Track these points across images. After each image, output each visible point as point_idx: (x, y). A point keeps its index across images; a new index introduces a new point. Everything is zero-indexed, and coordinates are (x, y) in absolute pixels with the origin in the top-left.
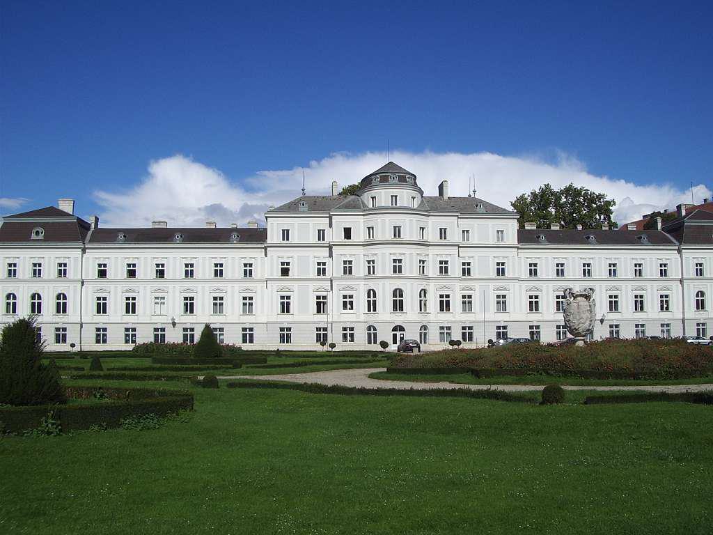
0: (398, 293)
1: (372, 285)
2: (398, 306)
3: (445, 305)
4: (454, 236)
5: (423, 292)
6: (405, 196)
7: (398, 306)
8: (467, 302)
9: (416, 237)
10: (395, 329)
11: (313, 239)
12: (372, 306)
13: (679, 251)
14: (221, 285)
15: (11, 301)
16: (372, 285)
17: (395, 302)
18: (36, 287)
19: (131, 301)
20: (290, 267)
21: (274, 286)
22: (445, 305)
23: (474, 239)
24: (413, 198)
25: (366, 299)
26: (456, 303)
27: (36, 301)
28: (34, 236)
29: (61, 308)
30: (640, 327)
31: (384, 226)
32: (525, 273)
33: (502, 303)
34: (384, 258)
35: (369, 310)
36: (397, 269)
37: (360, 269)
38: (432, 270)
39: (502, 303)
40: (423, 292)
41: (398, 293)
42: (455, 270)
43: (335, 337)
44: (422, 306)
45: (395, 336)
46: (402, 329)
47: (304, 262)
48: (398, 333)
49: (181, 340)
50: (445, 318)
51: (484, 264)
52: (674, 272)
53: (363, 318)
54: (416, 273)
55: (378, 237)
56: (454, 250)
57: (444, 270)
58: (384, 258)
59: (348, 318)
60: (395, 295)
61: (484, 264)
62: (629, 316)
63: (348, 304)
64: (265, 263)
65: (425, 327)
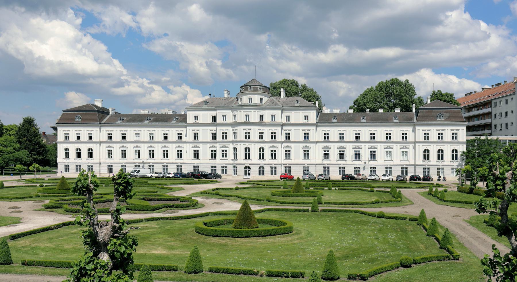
0: (247, 149)
1: (247, 145)
2: (247, 156)
4: (267, 119)
7: (247, 156)
15: (426, 153)
17: (246, 154)
18: (78, 145)
19: (196, 152)
20: (360, 135)
21: (104, 145)
23: (200, 121)
25: (258, 152)
27: (247, 152)
28: (77, 120)
29: (91, 155)
30: (165, 168)
32: (353, 139)
33: (306, 154)
36: (247, 136)
38: (267, 137)
39: (306, 154)
45: (246, 171)
46: (249, 168)
47: (205, 134)
48: (247, 170)
49: (192, 171)
50: (274, 162)
51: (297, 134)
52: (410, 138)
53: (231, 162)
55: (252, 120)
56: (230, 128)
59: (224, 162)
60: (246, 150)
61: (297, 134)
64: (188, 133)
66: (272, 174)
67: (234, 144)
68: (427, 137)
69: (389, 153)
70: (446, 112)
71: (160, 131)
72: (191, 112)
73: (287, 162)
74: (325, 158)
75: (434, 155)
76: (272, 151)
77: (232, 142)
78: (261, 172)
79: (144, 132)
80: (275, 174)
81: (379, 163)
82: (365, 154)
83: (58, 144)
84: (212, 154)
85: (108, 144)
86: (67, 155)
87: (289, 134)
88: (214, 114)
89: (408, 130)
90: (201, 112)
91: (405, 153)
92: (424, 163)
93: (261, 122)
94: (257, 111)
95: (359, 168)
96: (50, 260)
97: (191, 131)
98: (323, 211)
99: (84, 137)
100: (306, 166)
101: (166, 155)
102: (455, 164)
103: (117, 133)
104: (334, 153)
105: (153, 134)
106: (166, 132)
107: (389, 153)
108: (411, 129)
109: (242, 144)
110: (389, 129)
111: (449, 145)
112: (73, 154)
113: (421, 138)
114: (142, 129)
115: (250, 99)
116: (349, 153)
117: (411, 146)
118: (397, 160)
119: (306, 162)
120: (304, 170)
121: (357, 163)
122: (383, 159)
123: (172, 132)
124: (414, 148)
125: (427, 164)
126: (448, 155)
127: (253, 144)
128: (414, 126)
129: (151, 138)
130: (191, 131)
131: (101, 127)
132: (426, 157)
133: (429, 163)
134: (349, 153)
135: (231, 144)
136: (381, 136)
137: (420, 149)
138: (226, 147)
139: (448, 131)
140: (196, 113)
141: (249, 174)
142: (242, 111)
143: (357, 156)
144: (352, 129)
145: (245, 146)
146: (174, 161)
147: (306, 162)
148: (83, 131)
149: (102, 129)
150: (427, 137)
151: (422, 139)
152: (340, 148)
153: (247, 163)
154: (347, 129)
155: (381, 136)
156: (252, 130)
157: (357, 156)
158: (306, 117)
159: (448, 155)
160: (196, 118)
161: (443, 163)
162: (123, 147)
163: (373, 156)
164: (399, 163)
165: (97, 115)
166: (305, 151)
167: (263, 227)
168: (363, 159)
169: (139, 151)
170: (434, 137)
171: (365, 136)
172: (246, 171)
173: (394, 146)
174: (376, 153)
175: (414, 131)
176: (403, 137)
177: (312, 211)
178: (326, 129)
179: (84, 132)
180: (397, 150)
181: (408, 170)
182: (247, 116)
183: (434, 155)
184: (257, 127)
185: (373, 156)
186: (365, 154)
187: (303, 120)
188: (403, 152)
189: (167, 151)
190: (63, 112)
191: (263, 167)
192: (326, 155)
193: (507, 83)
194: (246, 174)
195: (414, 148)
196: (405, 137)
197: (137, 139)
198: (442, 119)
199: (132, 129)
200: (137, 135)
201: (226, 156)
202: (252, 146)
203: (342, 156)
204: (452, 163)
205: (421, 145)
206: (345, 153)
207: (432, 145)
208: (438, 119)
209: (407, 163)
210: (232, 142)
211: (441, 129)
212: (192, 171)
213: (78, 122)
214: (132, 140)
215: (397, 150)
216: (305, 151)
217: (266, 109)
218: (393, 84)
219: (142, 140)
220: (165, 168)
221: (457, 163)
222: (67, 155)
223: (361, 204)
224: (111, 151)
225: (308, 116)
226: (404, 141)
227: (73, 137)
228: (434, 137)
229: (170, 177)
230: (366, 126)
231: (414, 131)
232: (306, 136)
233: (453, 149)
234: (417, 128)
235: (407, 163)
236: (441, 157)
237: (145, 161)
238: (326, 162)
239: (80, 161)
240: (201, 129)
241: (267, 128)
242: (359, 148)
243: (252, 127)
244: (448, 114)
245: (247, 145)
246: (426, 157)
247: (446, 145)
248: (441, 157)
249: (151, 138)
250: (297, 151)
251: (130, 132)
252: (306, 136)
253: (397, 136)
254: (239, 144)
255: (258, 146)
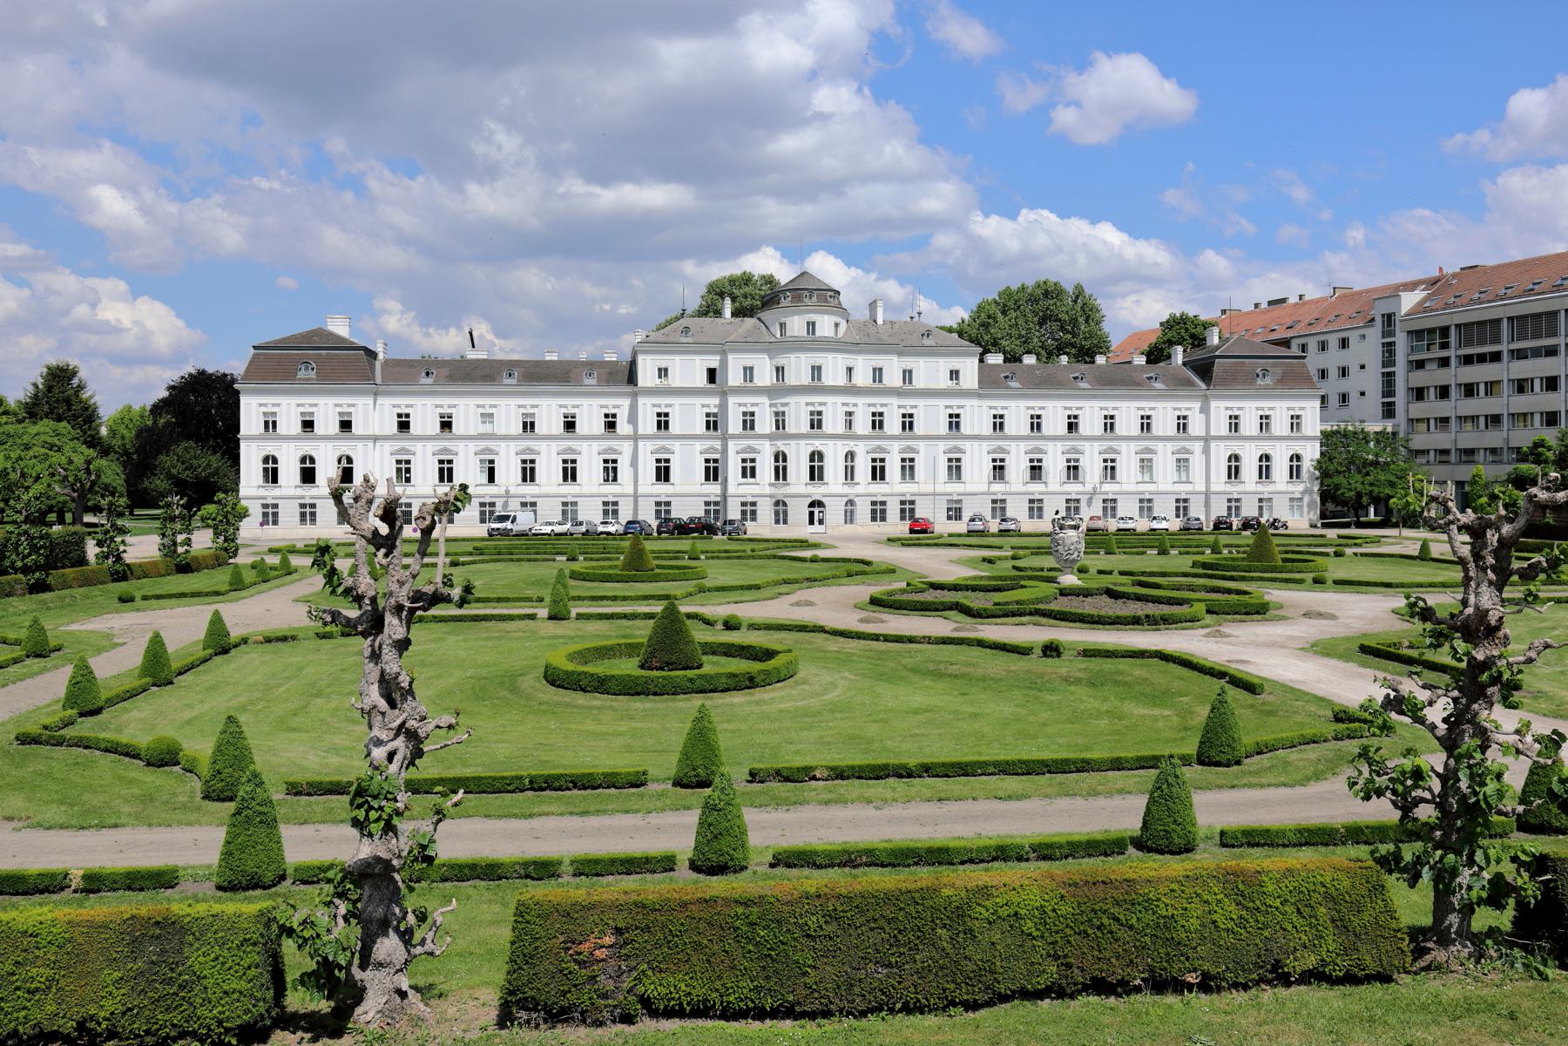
0: (817, 456)
1: (818, 445)
2: (816, 474)
3: (878, 473)
4: (893, 379)
5: (850, 456)
6: (826, 325)
7: (816, 474)
8: (908, 468)
9: (841, 380)
10: (812, 505)
11: (701, 380)
12: (781, 473)
13: (1206, 400)
14: (614, 444)
16: (781, 445)
18: (307, 447)
20: (411, 419)
22: (878, 473)
23: (675, 380)
24: (837, 325)
25: (773, 464)
26: (893, 469)
28: (301, 374)
30: (569, 509)
31: (798, 368)
33: (955, 468)
34: (798, 412)
35: (777, 478)
36: (816, 423)
37: (765, 424)
38: (862, 425)
39: (955, 468)
40: (850, 456)
41: (817, 456)
42: (893, 425)
43: (1127, 508)
44: (850, 473)
47: (689, 416)
48: (816, 511)
49: (701, 514)
50: (879, 489)
51: (931, 416)
52: (1196, 426)
53: (768, 490)
54: (840, 429)
55: (791, 379)
56: (764, 400)
57: (878, 422)
58: (798, 412)
59: (749, 489)
60: (777, 460)
61: (931, 416)
62: (553, 490)
63: (749, 471)
65: (851, 502)
66: (874, 519)
67: (779, 443)
68: (1235, 423)
69: (1146, 465)
70: (1274, 365)
71: (554, 408)
72: (649, 358)
73: (908, 489)
74: (1033, 478)
75: (1249, 468)
76: (874, 460)
77: (770, 437)
78: (781, 515)
79: (508, 410)
80: (1040, 517)
81: (1125, 488)
82: (1092, 466)
83: (243, 445)
84: (565, 470)
85: (606, 444)
86: (272, 476)
87: (820, 413)
88: (714, 361)
89: (1192, 408)
90: (677, 358)
91: (1182, 464)
92: (1229, 488)
93: (816, 386)
94: (840, 356)
95: (1078, 501)
96: (954, 760)
97: (649, 406)
98: (580, 617)
99: (327, 423)
100: (955, 497)
101: (570, 474)
102: (1298, 488)
103: (425, 413)
104: (1017, 467)
105: (274, 414)
106: (572, 411)
107: (1146, 465)
108: (1197, 405)
109: (803, 442)
110: (1146, 406)
111: (1284, 444)
112: (289, 472)
113: (1220, 426)
114: (502, 402)
115: (811, 326)
116: (1055, 465)
117: (1197, 447)
118: (1165, 480)
119: (955, 488)
120: (949, 509)
121: (1073, 488)
122: (1133, 480)
123: (590, 413)
124: (1206, 451)
125: (1234, 489)
126: (1280, 468)
127: (830, 443)
128: (1206, 400)
129: (529, 426)
130: (647, 410)
131: (376, 394)
132: (1234, 472)
133: (1240, 488)
134: (1055, 465)
135: (767, 443)
136: (1127, 421)
137: (1221, 453)
138: (754, 450)
139: (1281, 410)
140: (663, 360)
141: (821, 522)
142: (803, 356)
143: (1073, 470)
144: (1060, 404)
145: (811, 449)
146: (595, 489)
147: (955, 488)
148: (284, 407)
149: (380, 400)
150: (1235, 423)
151: (1224, 431)
152: (1031, 452)
153: (817, 491)
154: (1123, 405)
155: (1127, 421)
156: (830, 405)
157: (1073, 470)
158: (954, 374)
159: (1280, 468)
160: (663, 372)
161: (1271, 488)
162: (403, 451)
163: (1110, 471)
164: (1170, 488)
165: (345, 364)
166: (950, 460)
167: (712, 666)
168: (1088, 478)
169: (492, 462)
170: (1249, 426)
171: (1091, 422)
172: (811, 514)
173: (1159, 446)
174: (1117, 464)
175: (1205, 410)
176: (659, 423)
177: (551, 618)
178: (999, 405)
179: (327, 410)
180: (1164, 456)
181: (620, 508)
182: (817, 371)
183: (1249, 468)
184: (840, 399)
185: (1110, 471)
186: (1092, 466)
187: (944, 382)
188: (1179, 460)
189: (574, 461)
190: (253, 351)
191: (785, 504)
192: (999, 470)
193: (1307, 298)
194: (811, 522)
195: (1206, 451)
196: (1182, 425)
197: (487, 429)
198: (1268, 381)
199: (472, 402)
200: (487, 417)
201: (753, 475)
202: (790, 448)
203: (1036, 471)
204: (1291, 488)
205: (1222, 444)
206: (1044, 464)
207: (1247, 444)
208: (1259, 381)
209: (1188, 487)
210: (770, 437)
211: (1266, 405)
212: (701, 514)
213: (307, 381)
214: (473, 432)
215: (1164, 456)
216: (950, 460)
217: (859, 352)
218: (1046, 294)
219: (503, 432)
220: (569, 509)
221: (1301, 487)
222: (272, 476)
223: (508, 600)
224: (408, 462)
225: (666, 370)
226: (1035, 434)
227: (289, 423)
228: (1249, 426)
229: (608, 533)
230: (1094, 397)
231: (1205, 410)
232: (954, 422)
233: (338, 454)
234: (1214, 404)
235: (1188, 487)
236: (1265, 472)
237: (513, 491)
238: (998, 487)
239: (276, 492)
240: (677, 401)
241: (861, 401)
242: (1078, 452)
243: (829, 399)
244: (1279, 370)
245: (818, 445)
246: (1234, 472)
247: (1278, 444)
248: (1265, 472)
249: (529, 426)
250: (931, 459)
251: (466, 409)
252: (954, 422)
253: (1164, 421)
254: (793, 443)
255: (842, 447)
